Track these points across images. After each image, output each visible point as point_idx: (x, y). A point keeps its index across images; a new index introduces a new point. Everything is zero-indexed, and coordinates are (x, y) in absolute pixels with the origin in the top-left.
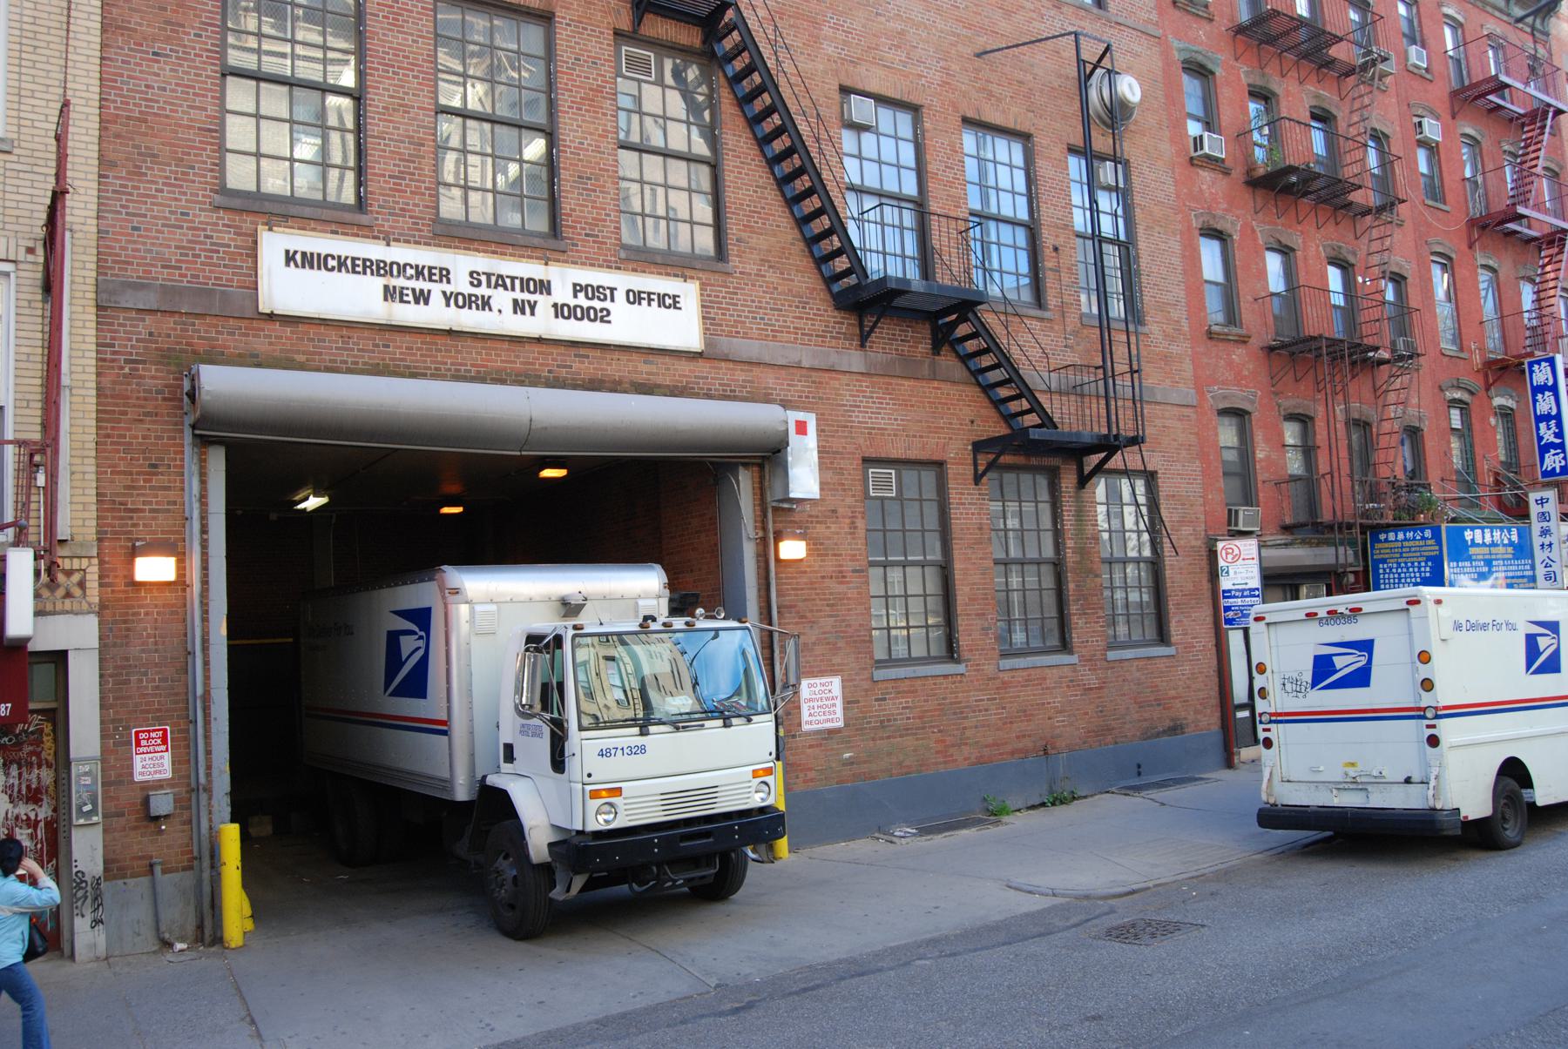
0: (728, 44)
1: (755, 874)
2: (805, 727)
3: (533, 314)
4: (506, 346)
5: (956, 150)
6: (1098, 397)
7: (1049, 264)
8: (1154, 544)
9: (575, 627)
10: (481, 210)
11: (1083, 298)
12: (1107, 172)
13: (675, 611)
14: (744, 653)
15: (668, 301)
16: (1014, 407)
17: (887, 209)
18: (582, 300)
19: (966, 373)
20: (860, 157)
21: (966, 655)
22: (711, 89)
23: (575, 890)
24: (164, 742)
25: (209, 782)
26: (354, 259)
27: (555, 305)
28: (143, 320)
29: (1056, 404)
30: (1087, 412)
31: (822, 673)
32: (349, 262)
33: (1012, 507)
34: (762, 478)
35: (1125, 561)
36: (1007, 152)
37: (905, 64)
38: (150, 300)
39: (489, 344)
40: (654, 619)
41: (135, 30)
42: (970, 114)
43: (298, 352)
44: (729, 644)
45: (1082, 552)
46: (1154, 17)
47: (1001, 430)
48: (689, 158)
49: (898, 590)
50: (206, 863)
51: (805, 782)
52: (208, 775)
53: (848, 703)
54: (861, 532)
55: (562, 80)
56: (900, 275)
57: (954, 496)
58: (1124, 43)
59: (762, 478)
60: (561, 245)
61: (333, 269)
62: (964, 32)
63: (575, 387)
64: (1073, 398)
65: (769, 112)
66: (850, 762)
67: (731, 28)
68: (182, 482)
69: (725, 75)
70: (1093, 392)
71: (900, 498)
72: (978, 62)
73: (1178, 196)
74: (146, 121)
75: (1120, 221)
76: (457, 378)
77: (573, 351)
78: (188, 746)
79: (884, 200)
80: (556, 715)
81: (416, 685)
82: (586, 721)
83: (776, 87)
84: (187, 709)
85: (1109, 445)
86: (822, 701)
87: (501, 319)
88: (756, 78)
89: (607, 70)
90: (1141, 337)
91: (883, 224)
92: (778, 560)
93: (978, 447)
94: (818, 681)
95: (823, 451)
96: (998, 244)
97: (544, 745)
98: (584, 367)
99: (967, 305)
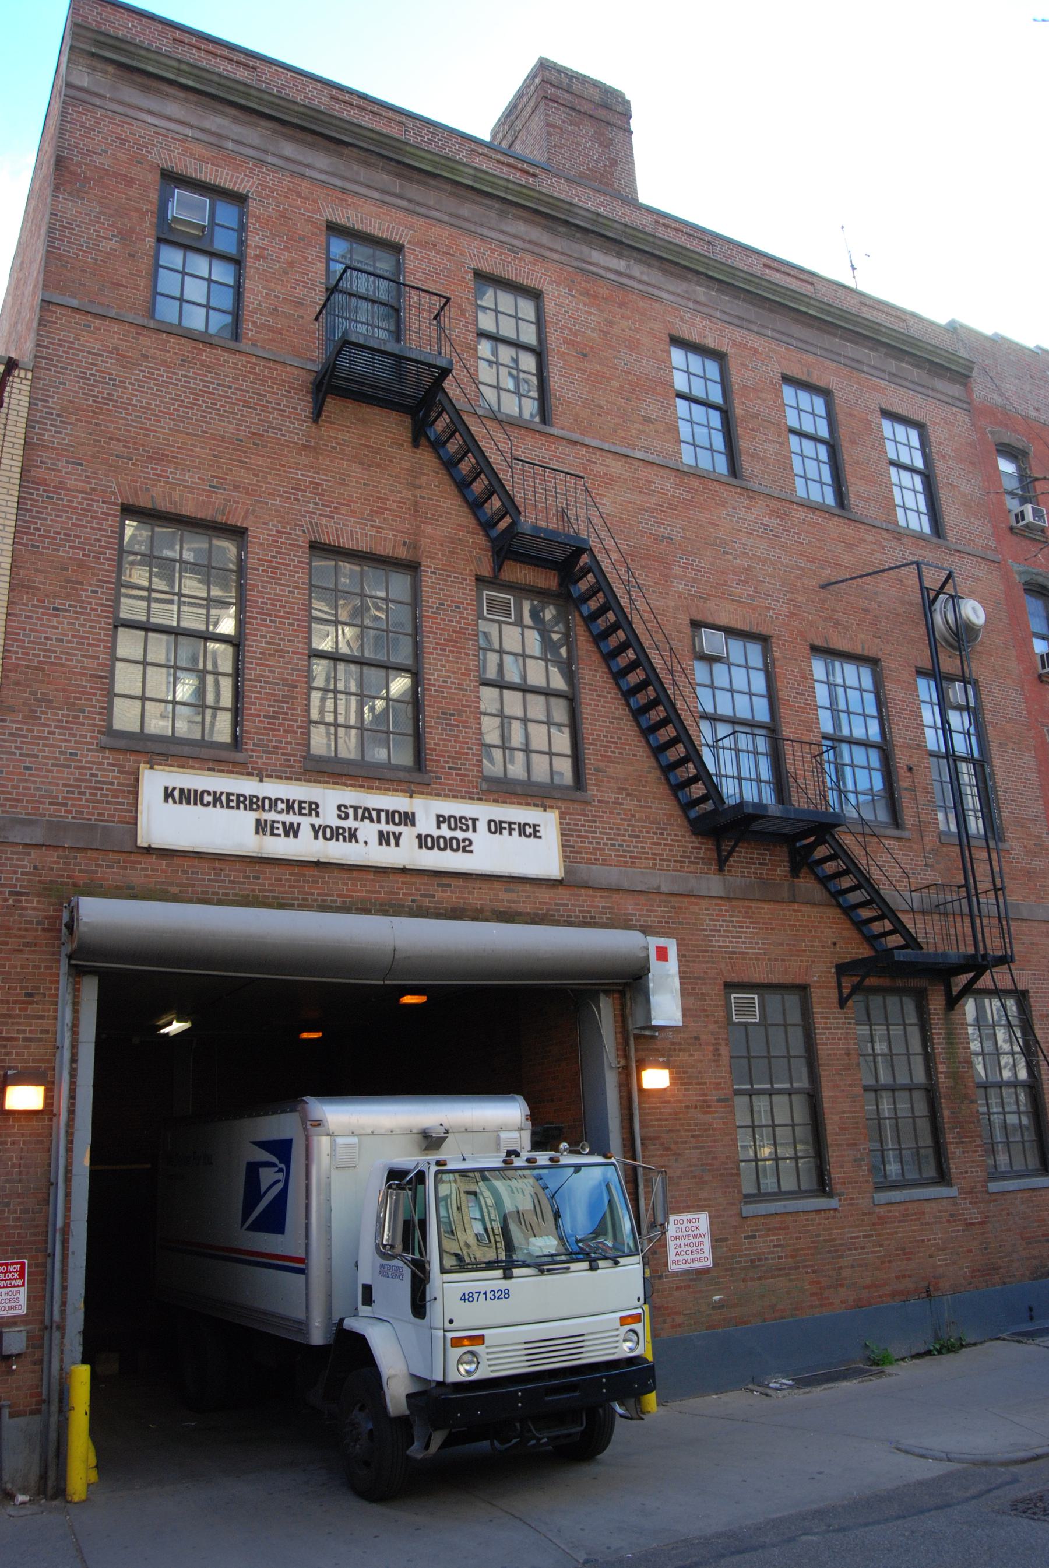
0: (583, 586)
1: (623, 1431)
2: (672, 1267)
3: (397, 845)
4: (371, 876)
5: (807, 677)
6: (962, 915)
7: (904, 784)
8: (1030, 1067)
9: (438, 1163)
10: (349, 747)
11: (941, 816)
12: (956, 692)
13: (537, 1145)
14: (608, 1186)
15: (529, 830)
16: (877, 928)
17: (741, 737)
18: (445, 831)
19: (826, 895)
20: (712, 687)
21: (839, 1188)
22: (568, 628)
23: (434, 1447)
24: (22, 1276)
25: (63, 1318)
26: (228, 795)
27: (419, 836)
28: (29, 854)
29: (920, 924)
30: (952, 931)
31: (688, 1209)
32: (224, 798)
33: (880, 1030)
34: (623, 1006)
35: (1000, 1085)
36: (850, 673)
37: (752, 598)
38: (36, 835)
39: (355, 875)
40: (518, 1155)
41: (39, 589)
42: (818, 642)
43: (172, 884)
44: (589, 1177)
45: (955, 1076)
46: (992, 543)
47: (864, 952)
48: (547, 693)
49: (765, 1120)
50: (54, 1408)
51: (673, 1327)
52: (63, 1312)
53: (716, 1241)
54: (725, 1060)
55: (427, 624)
56: (756, 800)
57: (819, 1021)
58: (966, 570)
59: (623, 1006)
60: (426, 778)
61: (208, 804)
62: (809, 565)
63: (438, 916)
64: (936, 917)
65: (623, 647)
66: (719, 1306)
67: (586, 571)
68: (56, 1011)
69: (581, 615)
70: (957, 911)
71: (764, 1023)
72: (824, 593)
73: (1029, 712)
74: (42, 669)
75: (973, 739)
76: (324, 908)
77: (436, 881)
78: (44, 1281)
79: (738, 728)
80: (417, 1256)
81: (274, 1219)
82: (450, 1262)
83: (630, 624)
84: (46, 1242)
85: (977, 965)
86: (690, 1239)
87: (367, 850)
88: (611, 616)
89: (470, 614)
90: (1002, 854)
91: (737, 750)
92: (641, 1089)
93: (842, 969)
94: (684, 1217)
95: (683, 977)
96: (852, 766)
97: (404, 1288)
98: (447, 897)
99: (824, 827)
